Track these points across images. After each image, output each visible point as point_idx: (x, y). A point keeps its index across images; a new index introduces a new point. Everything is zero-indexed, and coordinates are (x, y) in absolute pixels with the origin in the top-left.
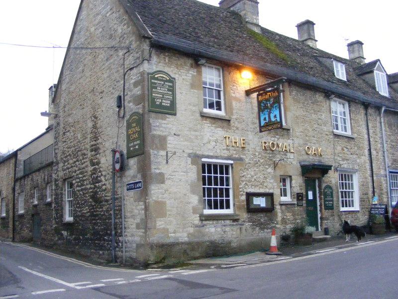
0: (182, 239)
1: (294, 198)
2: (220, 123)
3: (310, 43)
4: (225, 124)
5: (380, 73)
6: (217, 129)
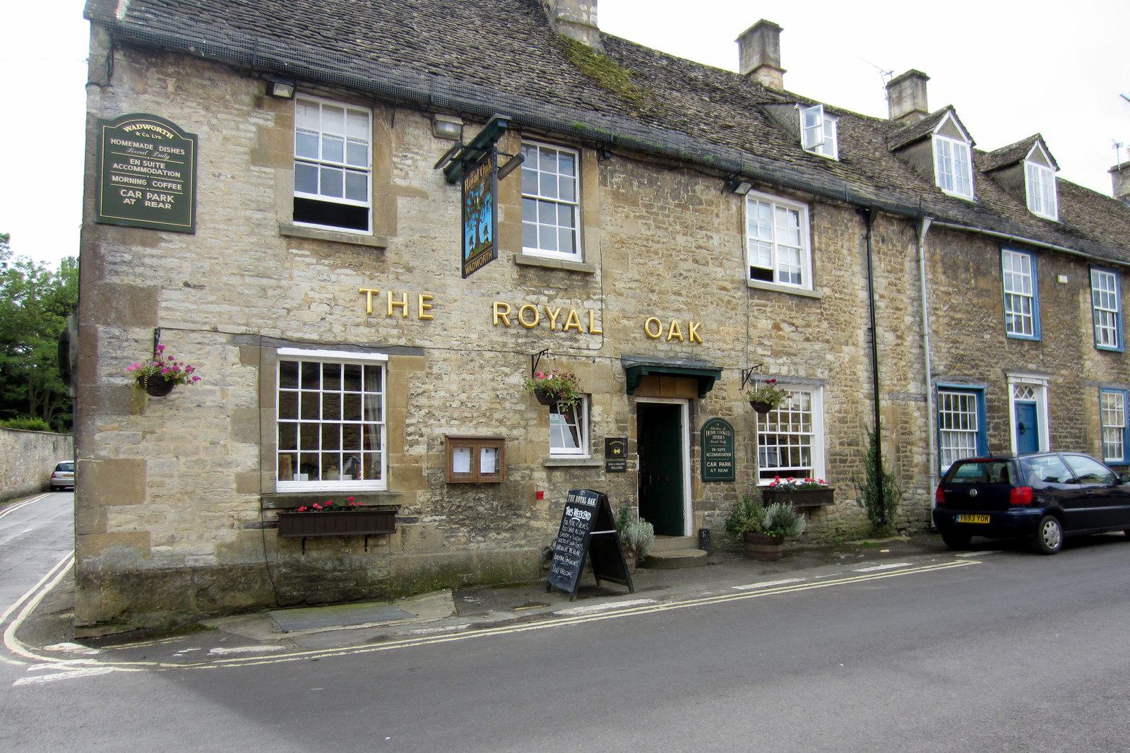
0: (196, 560)
1: (596, 451)
2: (349, 256)
3: (765, 78)
4: (366, 258)
5: (952, 142)
6: (338, 271)
